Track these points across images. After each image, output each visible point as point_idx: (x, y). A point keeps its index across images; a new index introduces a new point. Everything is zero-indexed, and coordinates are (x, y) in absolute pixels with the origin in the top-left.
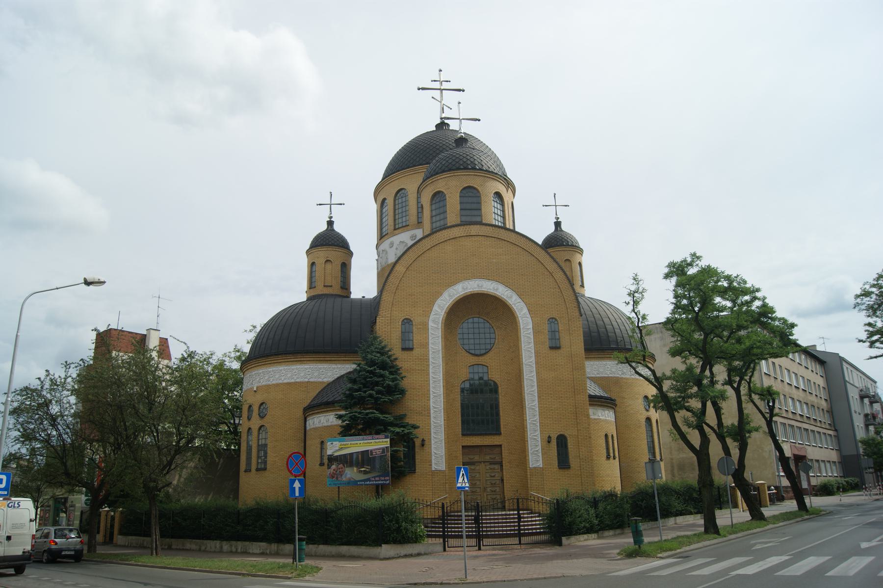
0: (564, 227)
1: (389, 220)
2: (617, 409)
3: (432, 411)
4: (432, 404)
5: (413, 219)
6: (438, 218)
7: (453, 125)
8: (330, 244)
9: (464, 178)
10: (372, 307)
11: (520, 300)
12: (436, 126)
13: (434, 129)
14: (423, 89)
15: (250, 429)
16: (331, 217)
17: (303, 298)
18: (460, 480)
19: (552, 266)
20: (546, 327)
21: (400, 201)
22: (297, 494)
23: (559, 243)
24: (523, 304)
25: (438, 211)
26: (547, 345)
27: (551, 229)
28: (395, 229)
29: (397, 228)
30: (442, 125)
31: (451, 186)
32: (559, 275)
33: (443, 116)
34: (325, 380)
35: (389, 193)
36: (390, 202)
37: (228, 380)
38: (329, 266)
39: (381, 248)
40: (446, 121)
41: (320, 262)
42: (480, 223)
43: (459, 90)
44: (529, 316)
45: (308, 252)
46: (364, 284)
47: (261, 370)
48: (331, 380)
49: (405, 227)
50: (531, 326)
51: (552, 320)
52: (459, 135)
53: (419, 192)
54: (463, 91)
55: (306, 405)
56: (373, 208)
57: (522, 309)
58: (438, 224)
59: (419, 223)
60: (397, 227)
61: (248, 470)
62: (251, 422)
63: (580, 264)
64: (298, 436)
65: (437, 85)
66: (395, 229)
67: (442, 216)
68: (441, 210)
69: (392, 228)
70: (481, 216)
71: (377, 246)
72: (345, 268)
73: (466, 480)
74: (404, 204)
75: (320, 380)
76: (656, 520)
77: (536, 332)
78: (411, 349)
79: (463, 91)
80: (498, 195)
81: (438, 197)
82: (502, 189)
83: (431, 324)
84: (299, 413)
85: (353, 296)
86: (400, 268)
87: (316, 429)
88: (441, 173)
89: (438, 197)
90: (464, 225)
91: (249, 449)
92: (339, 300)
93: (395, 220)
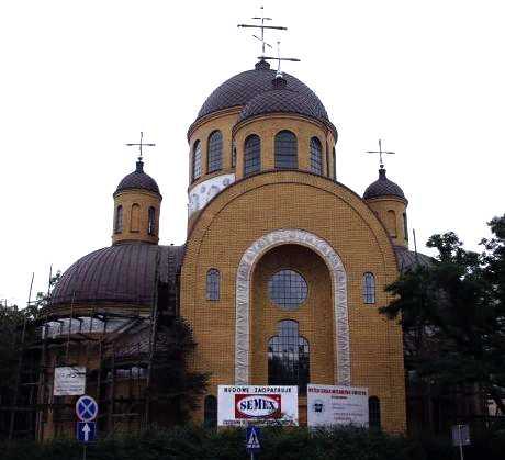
0: (388, 175)
1: (201, 162)
5: (226, 164)
7: (274, 65)
8: (139, 190)
9: (280, 121)
13: (254, 68)
17: (108, 243)
18: (251, 441)
19: (371, 219)
22: (86, 438)
23: (385, 194)
27: (376, 177)
29: (212, 172)
30: (263, 65)
31: (267, 131)
39: (192, 193)
41: (127, 205)
42: (295, 170)
46: (173, 230)
53: (235, 131)
56: (185, 149)
58: (250, 170)
63: (405, 215)
69: (204, 171)
71: (189, 190)
72: (154, 212)
74: (217, 152)
80: (316, 140)
81: (252, 140)
82: (320, 134)
85: (160, 243)
86: (208, 216)
88: (265, 119)
89: (252, 140)
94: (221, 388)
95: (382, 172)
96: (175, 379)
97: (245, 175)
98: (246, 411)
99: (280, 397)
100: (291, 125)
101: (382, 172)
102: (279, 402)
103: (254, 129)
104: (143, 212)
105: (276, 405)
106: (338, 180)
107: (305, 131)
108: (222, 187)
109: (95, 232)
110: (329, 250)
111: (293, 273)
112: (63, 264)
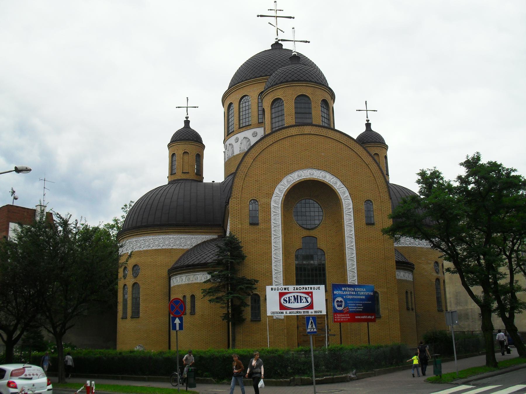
0: (373, 128)
1: (235, 120)
2: (414, 271)
3: (273, 273)
4: (273, 267)
5: (254, 120)
6: (277, 120)
7: (286, 46)
8: (187, 142)
10: (226, 189)
11: (343, 186)
12: (272, 46)
13: (270, 48)
14: (261, 16)
15: (125, 285)
16: (187, 118)
18: (310, 326)
19: (368, 160)
20: (363, 207)
21: (244, 105)
23: (472, 164)
24: (345, 189)
25: (277, 115)
26: (364, 221)
27: (363, 129)
28: (240, 128)
29: (242, 128)
30: (277, 46)
31: (288, 95)
32: (373, 166)
33: (280, 38)
34: (185, 247)
35: (235, 98)
36: (235, 106)
37: (98, 245)
38: (186, 157)
39: (228, 143)
40: (280, 42)
42: (311, 124)
43: (290, 17)
44: (350, 198)
45: (169, 146)
46: (214, 171)
47: (134, 240)
48: (189, 247)
49: (248, 127)
50: (351, 206)
51: (368, 202)
52: (293, 53)
54: (294, 18)
55: (171, 265)
57: (344, 193)
58: (277, 125)
59: (260, 124)
60: (241, 126)
61: (124, 317)
62: (126, 280)
63: (386, 157)
64: (159, 291)
65: (273, 13)
66: (240, 128)
67: (280, 118)
68: (280, 113)
69: (238, 126)
70: (311, 118)
72: (199, 158)
73: (314, 327)
75: (181, 247)
76: (453, 360)
77: (356, 211)
78: (257, 224)
79: (294, 18)
82: (328, 97)
83: (273, 204)
84: (165, 273)
85: (205, 181)
87: (179, 286)
88: (281, 85)
90: (299, 126)
91: (125, 301)
92: (194, 184)
93: (240, 120)
94: (268, 288)
95: (368, 125)
96: (234, 284)
97: (272, 128)
98: (287, 305)
99: (312, 293)
100: (307, 91)
101: (368, 125)
102: (312, 297)
103: (279, 94)
104: (192, 158)
105: (309, 300)
106: (336, 128)
107: (316, 96)
108: (253, 141)
109: (155, 173)
110: (339, 183)
111: (311, 201)
112: (136, 196)
